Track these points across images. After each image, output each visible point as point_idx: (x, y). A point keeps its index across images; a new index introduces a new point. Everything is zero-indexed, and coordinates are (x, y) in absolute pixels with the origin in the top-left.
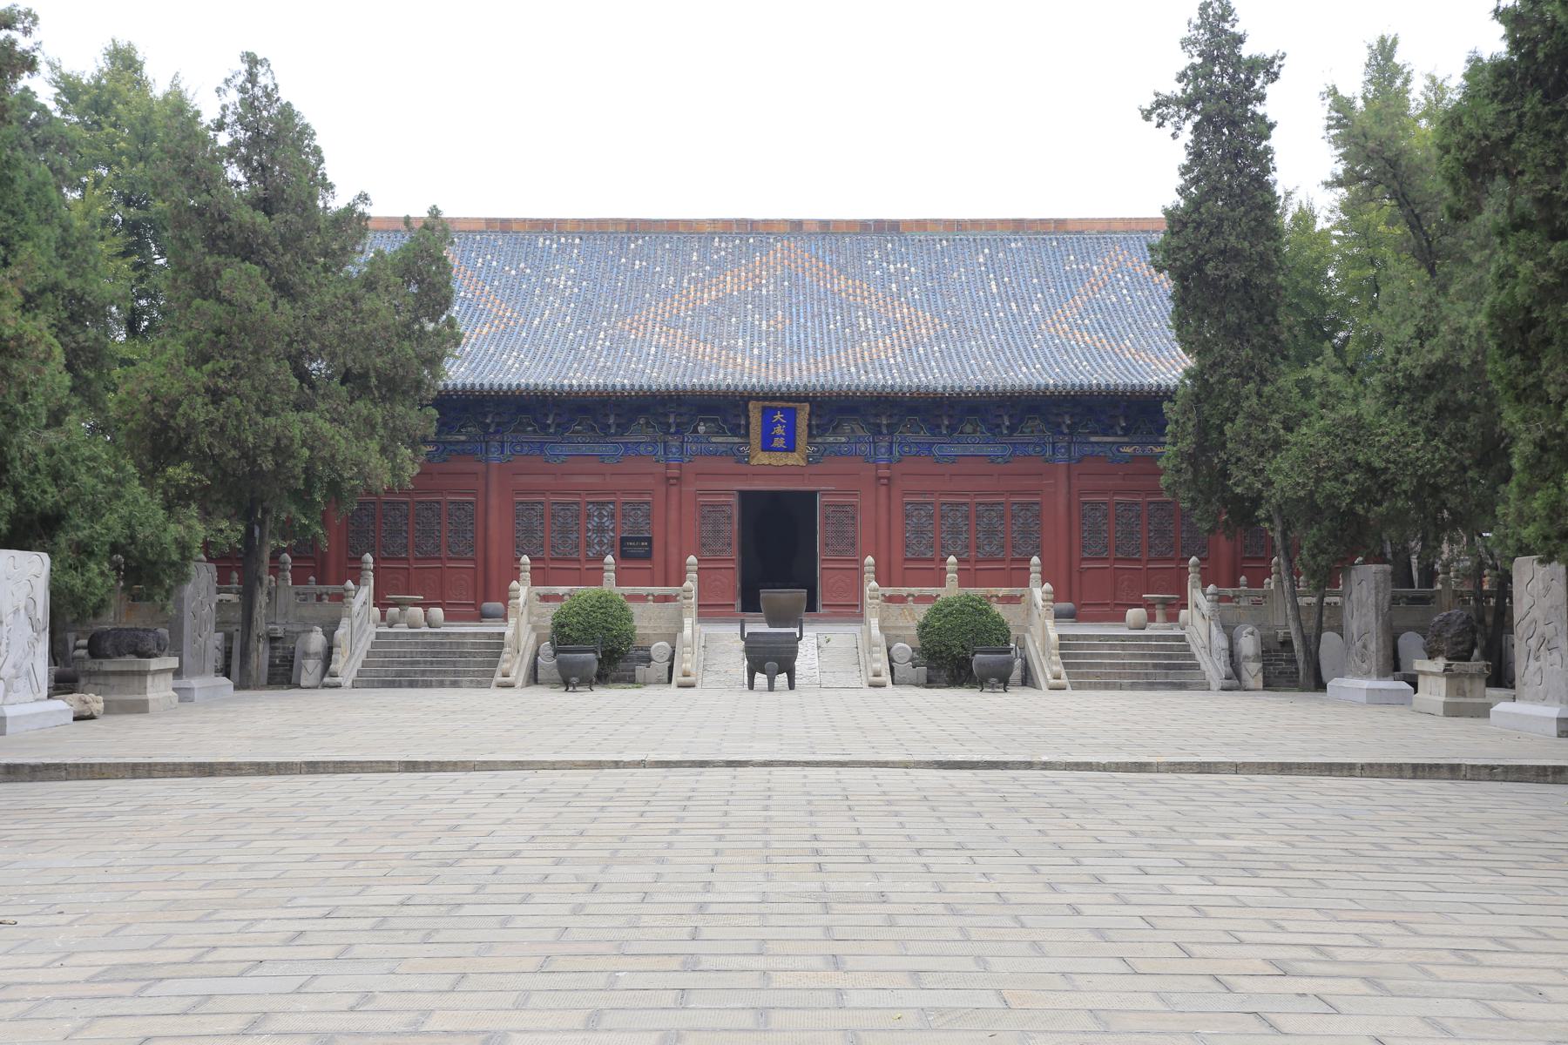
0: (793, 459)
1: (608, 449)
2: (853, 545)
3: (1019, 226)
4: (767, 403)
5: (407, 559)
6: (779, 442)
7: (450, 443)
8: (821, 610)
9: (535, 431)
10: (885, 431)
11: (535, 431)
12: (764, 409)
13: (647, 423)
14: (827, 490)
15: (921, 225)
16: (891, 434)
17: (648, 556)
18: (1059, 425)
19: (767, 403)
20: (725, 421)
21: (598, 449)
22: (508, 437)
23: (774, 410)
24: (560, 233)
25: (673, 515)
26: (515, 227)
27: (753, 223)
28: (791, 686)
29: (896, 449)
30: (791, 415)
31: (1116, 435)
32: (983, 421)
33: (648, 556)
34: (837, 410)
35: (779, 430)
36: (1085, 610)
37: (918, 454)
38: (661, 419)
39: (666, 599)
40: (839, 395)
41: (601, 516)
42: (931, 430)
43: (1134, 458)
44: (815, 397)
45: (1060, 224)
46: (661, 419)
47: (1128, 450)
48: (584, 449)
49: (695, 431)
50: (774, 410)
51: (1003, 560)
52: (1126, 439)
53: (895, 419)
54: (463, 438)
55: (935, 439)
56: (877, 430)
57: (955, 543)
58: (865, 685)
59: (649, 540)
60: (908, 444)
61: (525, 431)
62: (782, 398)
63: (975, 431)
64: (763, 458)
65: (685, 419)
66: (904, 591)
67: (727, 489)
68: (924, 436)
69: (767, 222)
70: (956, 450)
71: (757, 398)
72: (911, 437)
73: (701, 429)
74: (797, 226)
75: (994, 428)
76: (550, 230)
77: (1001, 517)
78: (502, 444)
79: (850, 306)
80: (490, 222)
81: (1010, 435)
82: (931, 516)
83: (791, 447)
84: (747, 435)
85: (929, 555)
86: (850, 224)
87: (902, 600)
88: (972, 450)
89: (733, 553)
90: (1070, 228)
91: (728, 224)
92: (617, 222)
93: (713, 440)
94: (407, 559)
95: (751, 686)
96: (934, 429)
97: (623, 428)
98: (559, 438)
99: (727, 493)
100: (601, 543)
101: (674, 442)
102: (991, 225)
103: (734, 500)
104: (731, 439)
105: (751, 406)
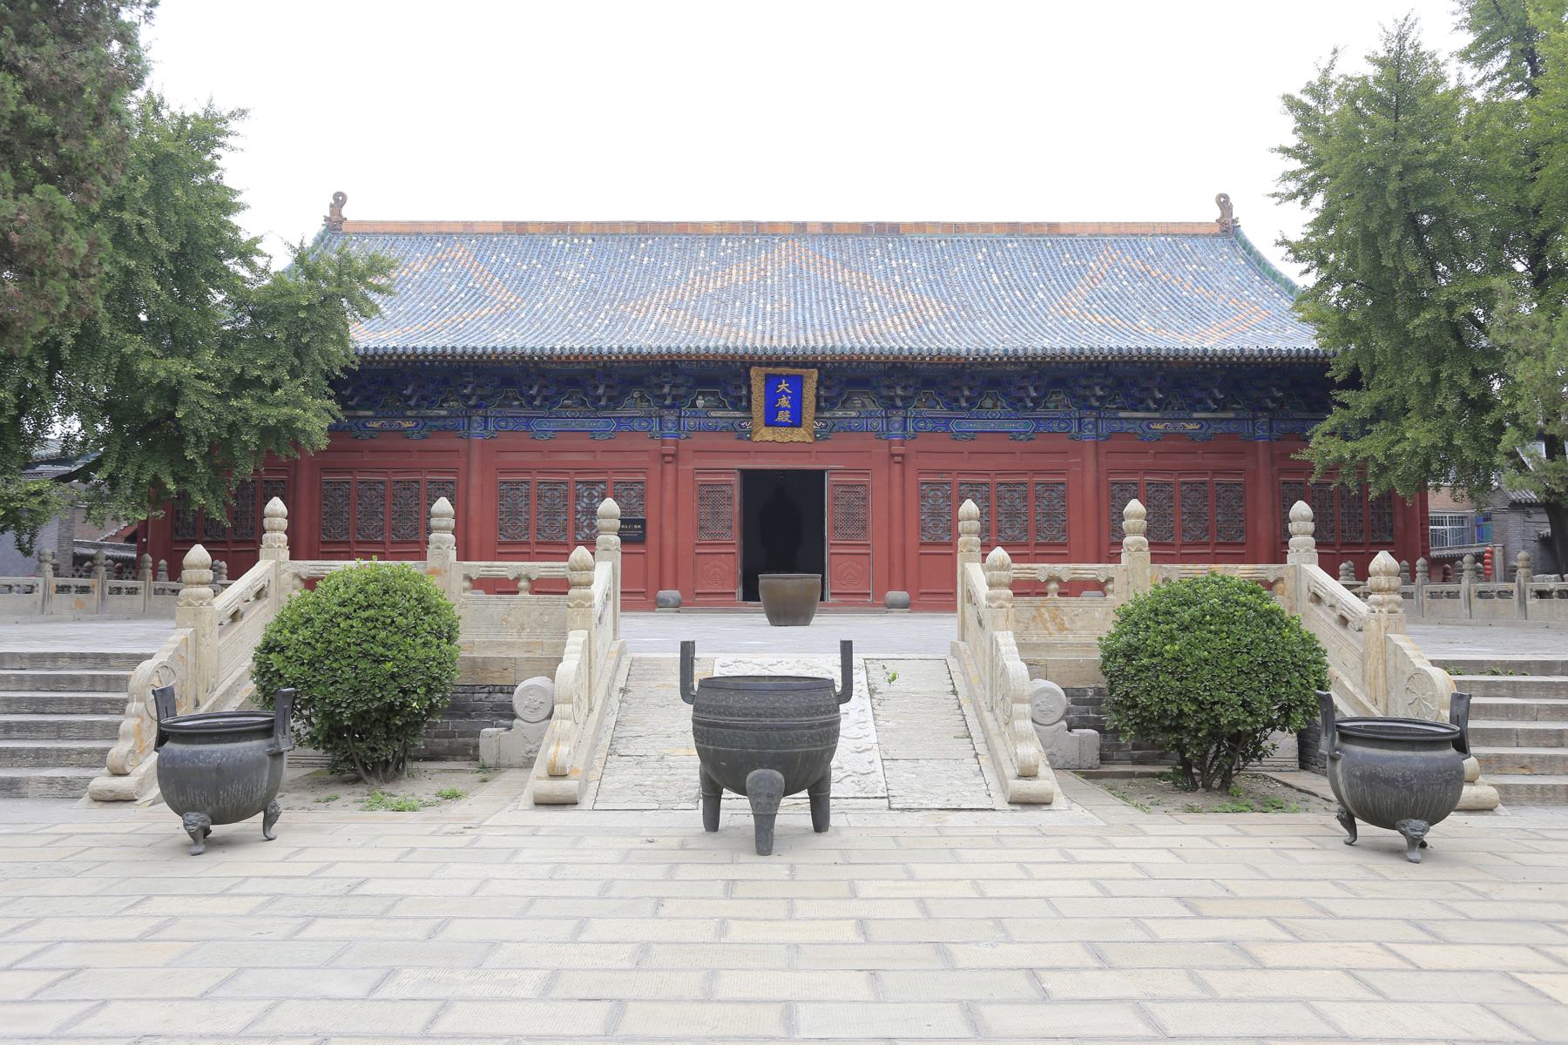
0: (800, 435)
1: (601, 425)
2: (864, 528)
3: (1013, 229)
4: (770, 370)
5: (383, 543)
6: (784, 416)
7: (431, 418)
8: (829, 599)
9: (521, 406)
10: (899, 403)
11: (521, 406)
12: (768, 377)
13: (642, 397)
14: (835, 466)
15: (920, 227)
16: (905, 408)
18: (892, 399)
19: (770, 370)
20: (726, 394)
21: (588, 424)
22: (491, 412)
23: (777, 379)
24: (573, 234)
25: (669, 495)
26: (530, 229)
27: (759, 224)
28: (820, 822)
29: (910, 424)
30: (797, 383)
31: (1148, 409)
32: (1005, 395)
34: (852, 379)
35: (784, 402)
40: (850, 362)
42: (948, 405)
43: (1166, 435)
44: (823, 363)
45: (1053, 227)
47: (1160, 427)
48: (574, 424)
49: (694, 405)
50: (777, 379)
52: (1157, 415)
53: (910, 392)
54: (443, 413)
58: (999, 801)
59: (643, 522)
60: (924, 419)
61: (511, 406)
62: (787, 364)
63: (995, 406)
64: (767, 434)
65: (682, 391)
67: (728, 468)
68: (941, 411)
69: (771, 224)
70: (976, 426)
71: (760, 364)
72: (926, 412)
73: (700, 402)
74: (801, 228)
75: (1016, 403)
76: (564, 232)
77: (1025, 498)
79: (854, 294)
80: (507, 225)
81: (1033, 409)
82: (948, 497)
83: (796, 422)
84: (749, 408)
86: (851, 225)
88: (992, 425)
89: (734, 537)
90: (1063, 230)
91: (734, 225)
92: (628, 224)
93: (713, 414)
94: (383, 543)
95: (712, 821)
96: (952, 403)
97: (615, 401)
98: (544, 413)
101: (670, 417)
102: (987, 227)
103: (735, 480)
104: (732, 414)
105: (753, 372)
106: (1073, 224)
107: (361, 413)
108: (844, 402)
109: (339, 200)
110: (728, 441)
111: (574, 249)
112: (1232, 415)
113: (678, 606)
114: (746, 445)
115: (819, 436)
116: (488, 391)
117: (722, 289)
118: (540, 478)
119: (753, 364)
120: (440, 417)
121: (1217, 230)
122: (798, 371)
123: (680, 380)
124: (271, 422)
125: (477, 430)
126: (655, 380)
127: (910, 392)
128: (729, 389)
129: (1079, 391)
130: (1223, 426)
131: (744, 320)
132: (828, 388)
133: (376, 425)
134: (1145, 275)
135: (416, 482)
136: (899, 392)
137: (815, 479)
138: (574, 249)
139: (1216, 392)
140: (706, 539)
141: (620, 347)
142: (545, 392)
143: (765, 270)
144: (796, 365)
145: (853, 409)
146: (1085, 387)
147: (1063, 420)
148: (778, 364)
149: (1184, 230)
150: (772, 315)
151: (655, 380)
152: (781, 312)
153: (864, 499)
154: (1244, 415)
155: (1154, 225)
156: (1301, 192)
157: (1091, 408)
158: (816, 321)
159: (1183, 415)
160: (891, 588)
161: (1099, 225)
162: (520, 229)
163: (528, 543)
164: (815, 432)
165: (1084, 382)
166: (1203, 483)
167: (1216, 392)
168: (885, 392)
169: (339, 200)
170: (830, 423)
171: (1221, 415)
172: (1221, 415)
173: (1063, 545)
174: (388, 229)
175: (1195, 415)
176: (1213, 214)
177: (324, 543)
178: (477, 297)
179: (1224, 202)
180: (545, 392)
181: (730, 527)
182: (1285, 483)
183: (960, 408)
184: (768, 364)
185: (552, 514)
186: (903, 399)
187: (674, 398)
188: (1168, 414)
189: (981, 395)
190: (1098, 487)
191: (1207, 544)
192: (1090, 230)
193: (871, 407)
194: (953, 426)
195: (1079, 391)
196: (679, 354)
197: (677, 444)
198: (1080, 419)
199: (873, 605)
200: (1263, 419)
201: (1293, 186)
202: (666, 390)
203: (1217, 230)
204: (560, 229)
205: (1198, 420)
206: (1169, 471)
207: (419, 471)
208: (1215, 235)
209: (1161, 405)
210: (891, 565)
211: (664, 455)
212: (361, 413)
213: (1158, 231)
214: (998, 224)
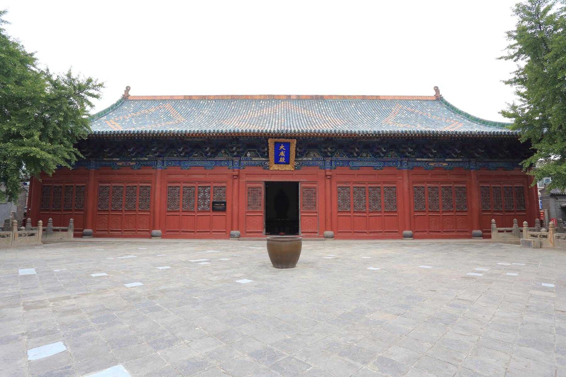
0: (289, 167)
1: (209, 163)
2: (315, 205)
4: (277, 140)
6: (282, 160)
7: (142, 161)
9: (177, 156)
10: (329, 154)
11: (177, 156)
13: (225, 153)
15: (331, 97)
16: (331, 157)
17: (224, 210)
18: (326, 153)
19: (277, 140)
20: (259, 151)
21: (204, 163)
23: (280, 144)
24: (208, 100)
29: (333, 163)
30: (287, 145)
31: (428, 157)
32: (371, 152)
33: (224, 210)
35: (282, 154)
36: (416, 234)
37: (343, 166)
38: (230, 150)
39: (32, 235)
41: (204, 192)
43: (435, 168)
45: (378, 97)
46: (230, 150)
47: (432, 164)
48: (198, 163)
49: (246, 156)
51: (380, 212)
52: (431, 160)
53: (333, 150)
54: (147, 159)
55: (350, 159)
56: (325, 155)
57: (360, 204)
59: (225, 203)
60: (339, 161)
61: (173, 156)
63: (367, 156)
64: (275, 167)
65: (241, 150)
66: (57, 228)
68: (345, 158)
69: (278, 96)
70: (360, 164)
71: (272, 138)
72: (340, 158)
73: (249, 155)
74: (289, 97)
75: (376, 155)
77: (380, 193)
78: (163, 161)
79: (308, 117)
83: (287, 162)
85: (348, 210)
87: (503, 231)
88: (366, 164)
89: (262, 209)
90: (381, 98)
92: (228, 96)
93: (254, 159)
96: (350, 154)
97: (214, 154)
99: (259, 182)
100: (204, 204)
101: (236, 160)
102: (354, 97)
103: (262, 186)
105: (269, 141)
106: (385, 96)
107: (114, 159)
108: (306, 154)
109: (128, 89)
110: (260, 170)
111: (208, 104)
112: (461, 160)
113: (239, 237)
114: (267, 172)
115: (297, 168)
116: (164, 150)
117: (260, 116)
118: (184, 185)
119: (269, 137)
120: (145, 161)
121: (435, 98)
122: (288, 140)
123: (240, 145)
124: (38, 157)
125: (159, 165)
126: (230, 145)
127: (333, 150)
128: (261, 149)
129: (401, 150)
130: (457, 164)
131: (267, 125)
132: (300, 148)
133: (120, 164)
134: (413, 112)
135: (135, 186)
136: (329, 149)
137: (295, 185)
138: (208, 104)
139: (456, 150)
140: (250, 210)
141: (214, 130)
142: (186, 150)
143: (276, 110)
144: (287, 138)
145: (310, 157)
146: (404, 148)
147: (393, 162)
148: (280, 138)
149: (423, 98)
150: (278, 123)
151: (230, 145)
152: (281, 123)
153: (315, 193)
154: (466, 160)
155: (413, 97)
156: (515, 55)
157: (406, 157)
158: (295, 125)
159: (442, 160)
160: (326, 230)
161: (394, 96)
162: (190, 98)
163: (179, 211)
164: (295, 166)
165: (404, 146)
166: (450, 187)
167: (456, 150)
168: (323, 150)
169: (128, 89)
170: (301, 163)
171: (456, 160)
172: (456, 160)
173: (395, 212)
174: (144, 98)
175: (447, 160)
176: (433, 93)
177: (99, 211)
178: (170, 119)
179: (437, 89)
180: (186, 150)
181: (260, 205)
182: (482, 187)
183: (354, 157)
184: (276, 138)
185: (189, 200)
186: (331, 153)
187: (238, 153)
188: (436, 160)
189: (361, 152)
190: (409, 189)
191: (452, 211)
192: (391, 98)
193: (318, 156)
194: (350, 164)
195: (401, 150)
196: (238, 133)
197: (239, 171)
198: (401, 161)
199: (319, 237)
200: (473, 161)
201: (512, 52)
202: (234, 149)
203: (435, 98)
204: (204, 98)
205: (447, 162)
206: (437, 182)
207: (136, 182)
208: (434, 100)
209: (435, 156)
210: (326, 220)
211: (234, 176)
212: (114, 159)
213: (414, 99)
214: (358, 96)
